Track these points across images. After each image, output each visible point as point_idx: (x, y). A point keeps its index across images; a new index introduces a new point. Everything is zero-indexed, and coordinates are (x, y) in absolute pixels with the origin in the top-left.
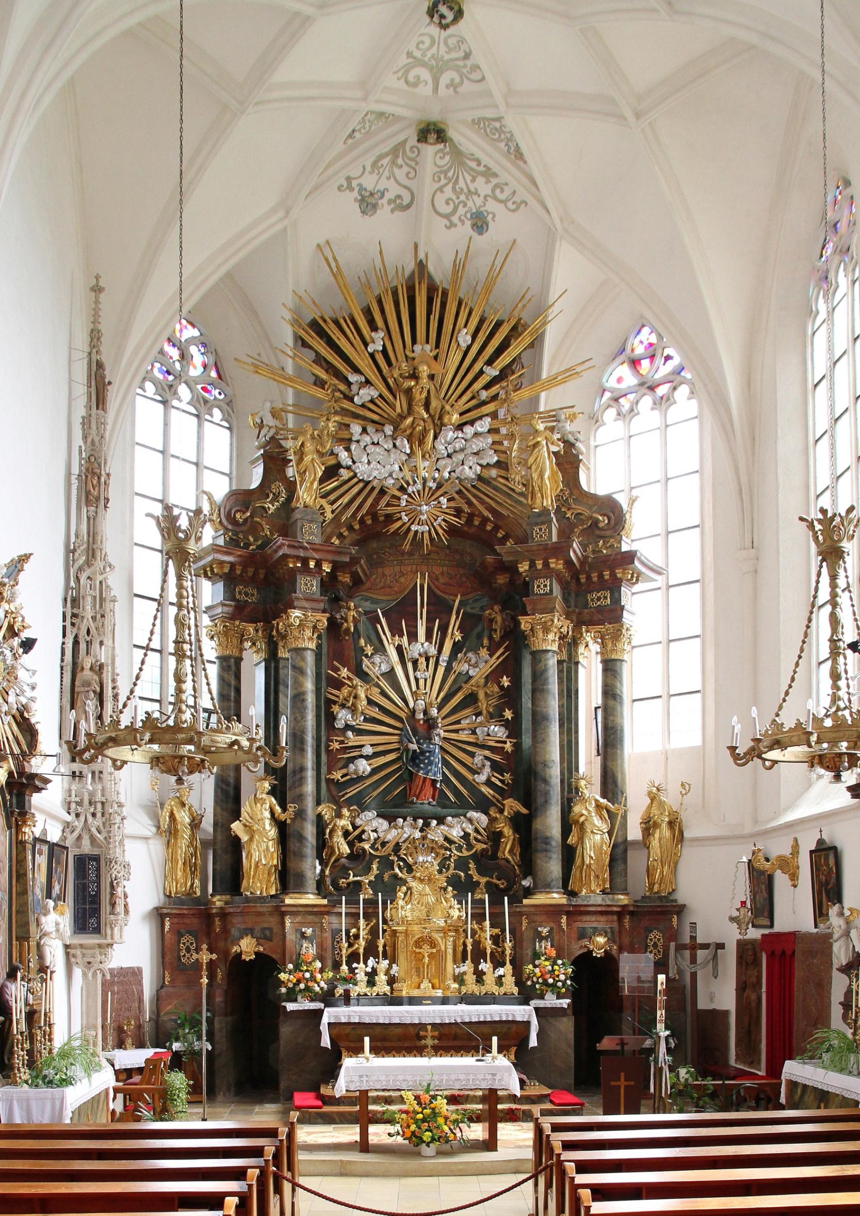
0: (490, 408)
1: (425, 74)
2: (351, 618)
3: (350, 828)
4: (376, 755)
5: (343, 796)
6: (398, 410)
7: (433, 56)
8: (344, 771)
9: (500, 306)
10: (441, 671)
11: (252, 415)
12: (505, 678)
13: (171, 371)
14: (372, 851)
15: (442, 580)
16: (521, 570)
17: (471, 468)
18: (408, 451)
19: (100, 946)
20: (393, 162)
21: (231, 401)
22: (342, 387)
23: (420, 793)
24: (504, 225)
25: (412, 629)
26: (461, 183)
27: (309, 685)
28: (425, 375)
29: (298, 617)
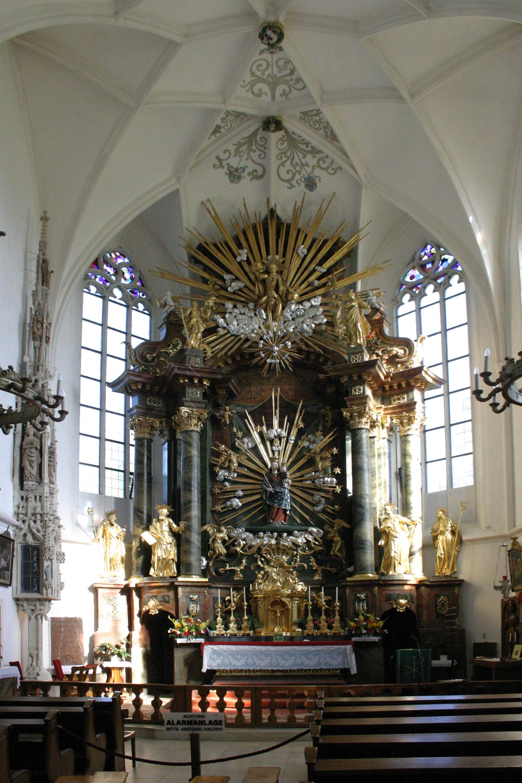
0: (322, 291)
1: (265, 88)
2: (227, 416)
3: (227, 538)
4: (245, 496)
5: (223, 520)
6: (257, 292)
7: (269, 75)
8: (223, 506)
9: (327, 229)
10: (290, 447)
11: (159, 300)
12: (335, 449)
13: (109, 280)
14: (241, 552)
15: (290, 394)
16: (342, 381)
17: (308, 325)
18: (265, 317)
19: (39, 600)
20: (249, 149)
21: (150, 299)
22: (220, 282)
23: (275, 517)
24: (326, 184)
25: (269, 422)
26: (296, 159)
27: (195, 452)
28: (274, 270)
29: (187, 412)
